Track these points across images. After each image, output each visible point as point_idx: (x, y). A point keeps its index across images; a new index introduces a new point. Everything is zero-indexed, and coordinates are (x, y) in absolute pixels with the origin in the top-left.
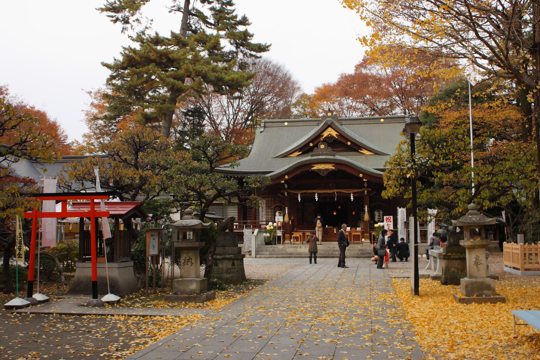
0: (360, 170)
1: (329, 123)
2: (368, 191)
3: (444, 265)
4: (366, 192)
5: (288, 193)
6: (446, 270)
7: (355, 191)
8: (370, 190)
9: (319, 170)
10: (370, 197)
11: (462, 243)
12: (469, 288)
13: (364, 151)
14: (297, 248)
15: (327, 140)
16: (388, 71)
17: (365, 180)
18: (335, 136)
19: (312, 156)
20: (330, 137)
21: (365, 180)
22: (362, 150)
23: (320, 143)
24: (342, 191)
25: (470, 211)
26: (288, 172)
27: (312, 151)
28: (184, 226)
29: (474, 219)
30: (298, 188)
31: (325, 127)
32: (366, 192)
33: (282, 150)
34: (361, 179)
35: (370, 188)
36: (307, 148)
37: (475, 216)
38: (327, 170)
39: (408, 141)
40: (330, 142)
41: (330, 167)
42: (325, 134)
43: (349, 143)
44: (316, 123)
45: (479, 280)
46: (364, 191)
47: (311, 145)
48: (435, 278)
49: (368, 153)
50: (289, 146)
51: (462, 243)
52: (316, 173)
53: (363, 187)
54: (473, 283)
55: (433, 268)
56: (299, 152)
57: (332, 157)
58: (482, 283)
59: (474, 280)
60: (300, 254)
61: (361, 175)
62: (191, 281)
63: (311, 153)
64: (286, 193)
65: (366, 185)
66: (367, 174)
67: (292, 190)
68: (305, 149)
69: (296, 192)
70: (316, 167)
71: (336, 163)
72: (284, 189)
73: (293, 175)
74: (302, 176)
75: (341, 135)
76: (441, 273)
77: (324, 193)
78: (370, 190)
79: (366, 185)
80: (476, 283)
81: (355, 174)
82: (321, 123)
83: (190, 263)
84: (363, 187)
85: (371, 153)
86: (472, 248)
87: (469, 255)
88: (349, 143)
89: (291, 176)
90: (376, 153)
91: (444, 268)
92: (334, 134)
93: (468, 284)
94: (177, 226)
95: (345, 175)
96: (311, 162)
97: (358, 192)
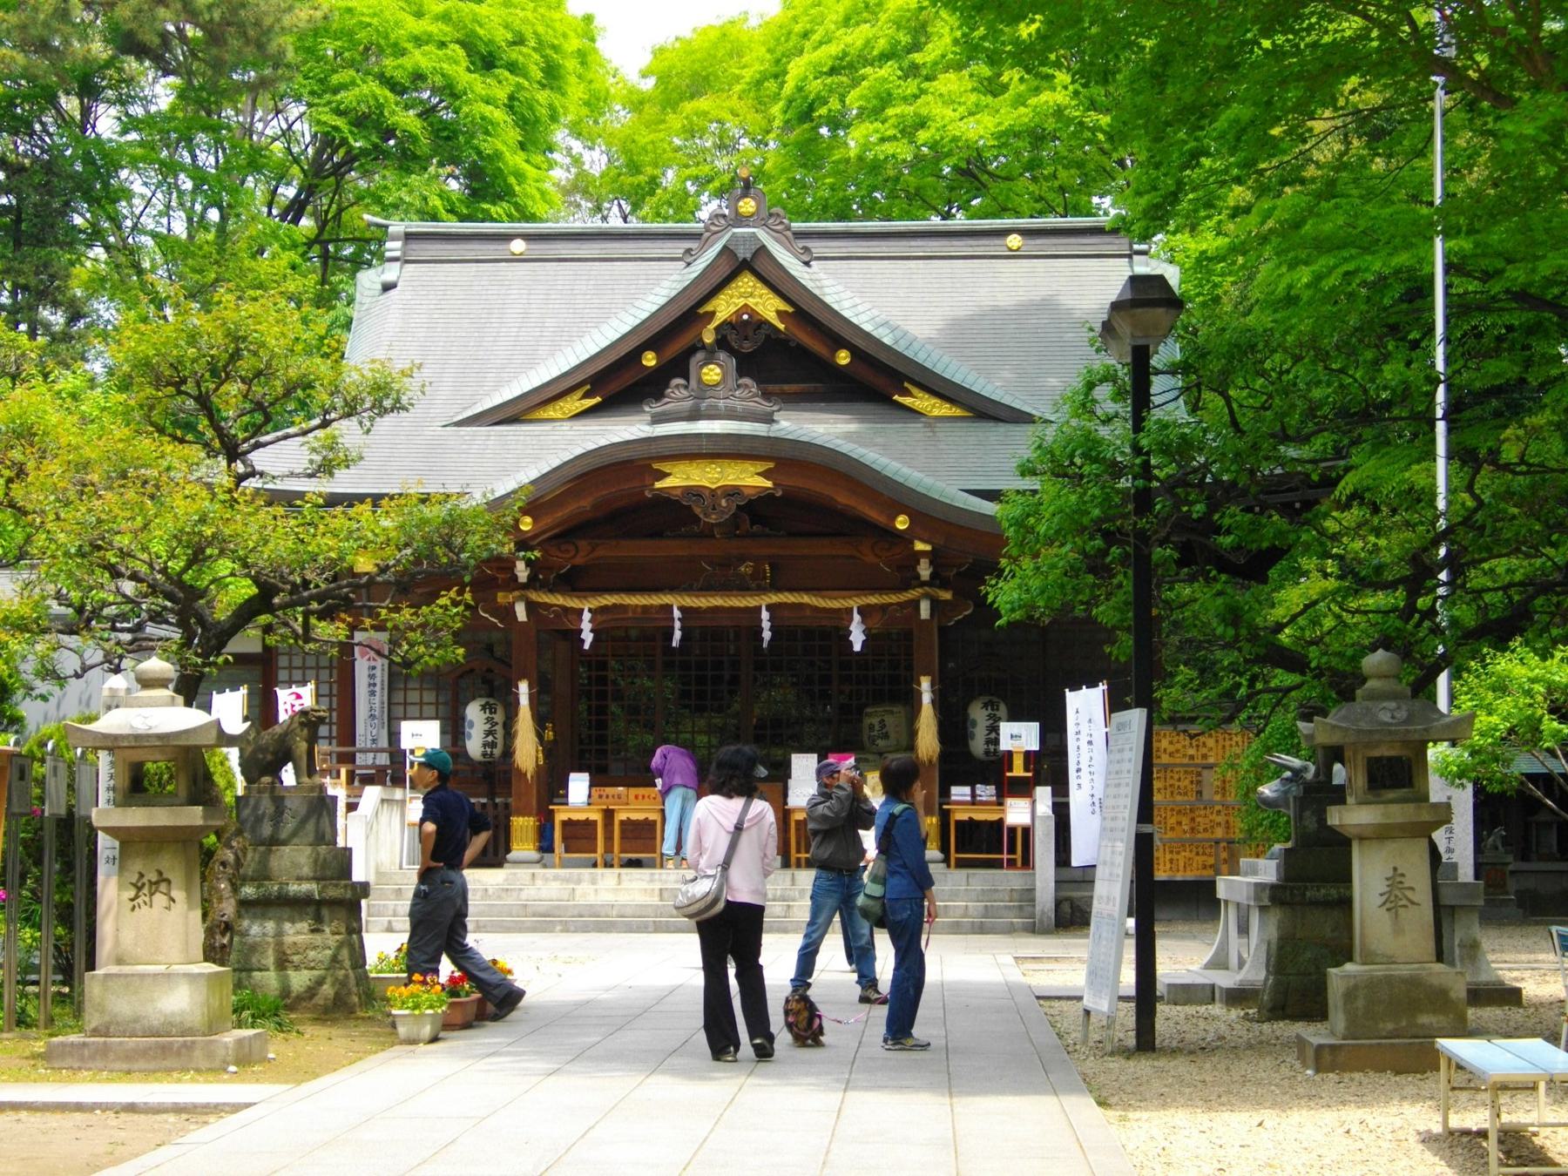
0: (896, 497)
1: (744, 253)
2: (936, 604)
3: (1273, 932)
4: (925, 610)
5: (531, 607)
6: (1282, 957)
7: (873, 600)
8: (947, 595)
9: (695, 492)
10: (943, 631)
11: (1336, 817)
12: (1360, 1003)
13: (920, 401)
14: (579, 881)
15: (732, 337)
16: (1006, 374)
17: (920, 546)
18: (771, 317)
19: (658, 419)
20: (746, 326)
21: (920, 546)
22: (907, 393)
23: (700, 356)
24: (806, 599)
25: (1370, 684)
26: (538, 500)
27: (659, 395)
28: (137, 737)
29: (1385, 717)
30: (573, 582)
31: (725, 270)
32: (925, 610)
33: (498, 386)
34: (904, 539)
35: (944, 585)
36: (628, 378)
37: (1393, 705)
38: (732, 492)
39: (1124, 374)
40: (747, 347)
41: (749, 477)
42: (724, 307)
43: (843, 358)
44: (678, 248)
45: (1403, 971)
46: (915, 604)
47: (650, 360)
48: (1236, 997)
49: (942, 409)
50: (531, 363)
51: (1336, 817)
52: (678, 512)
53: (908, 579)
54: (1372, 985)
55: (1234, 960)
56: (587, 395)
57: (759, 429)
58: (1413, 982)
59: (1378, 970)
60: (593, 911)
61: (902, 523)
62: (168, 976)
63: (657, 408)
64: (521, 613)
65: (925, 571)
66: (930, 515)
67: (551, 591)
68: (617, 381)
69: (572, 603)
70: (678, 477)
71: (787, 458)
72: (512, 583)
73: (560, 514)
74: (601, 518)
75: (809, 314)
76: (1262, 975)
77: (716, 609)
78: (947, 595)
79: (925, 571)
80: (1389, 980)
81: (874, 514)
82: (703, 249)
83: (160, 899)
84: (908, 579)
85: (957, 412)
86: (1382, 834)
87: (1362, 865)
88: (843, 358)
89: (547, 521)
90: (983, 411)
91: (1274, 947)
92: (769, 307)
93: (1356, 987)
94: (105, 736)
95: (815, 515)
96: (654, 450)
97: (883, 608)
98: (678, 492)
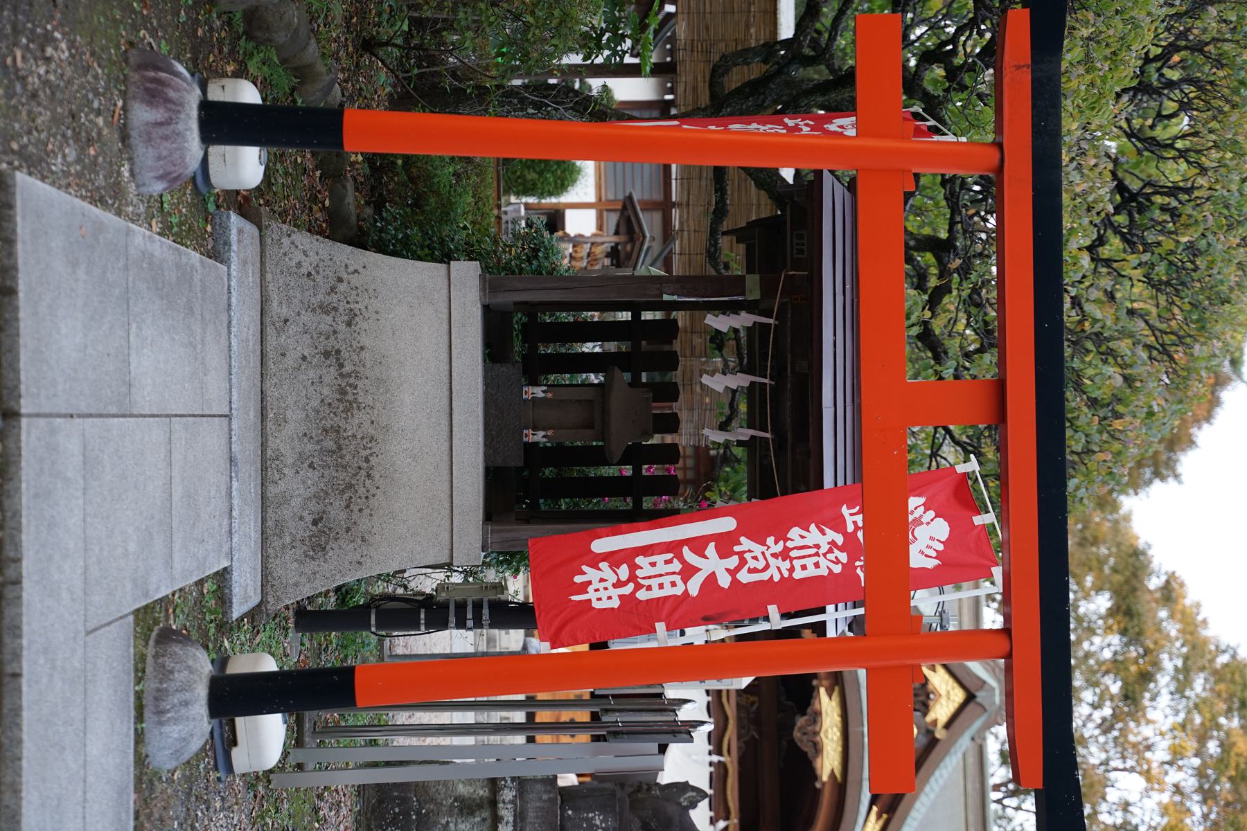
38: (818, 748)
41: (829, 762)
98: (817, 706)
